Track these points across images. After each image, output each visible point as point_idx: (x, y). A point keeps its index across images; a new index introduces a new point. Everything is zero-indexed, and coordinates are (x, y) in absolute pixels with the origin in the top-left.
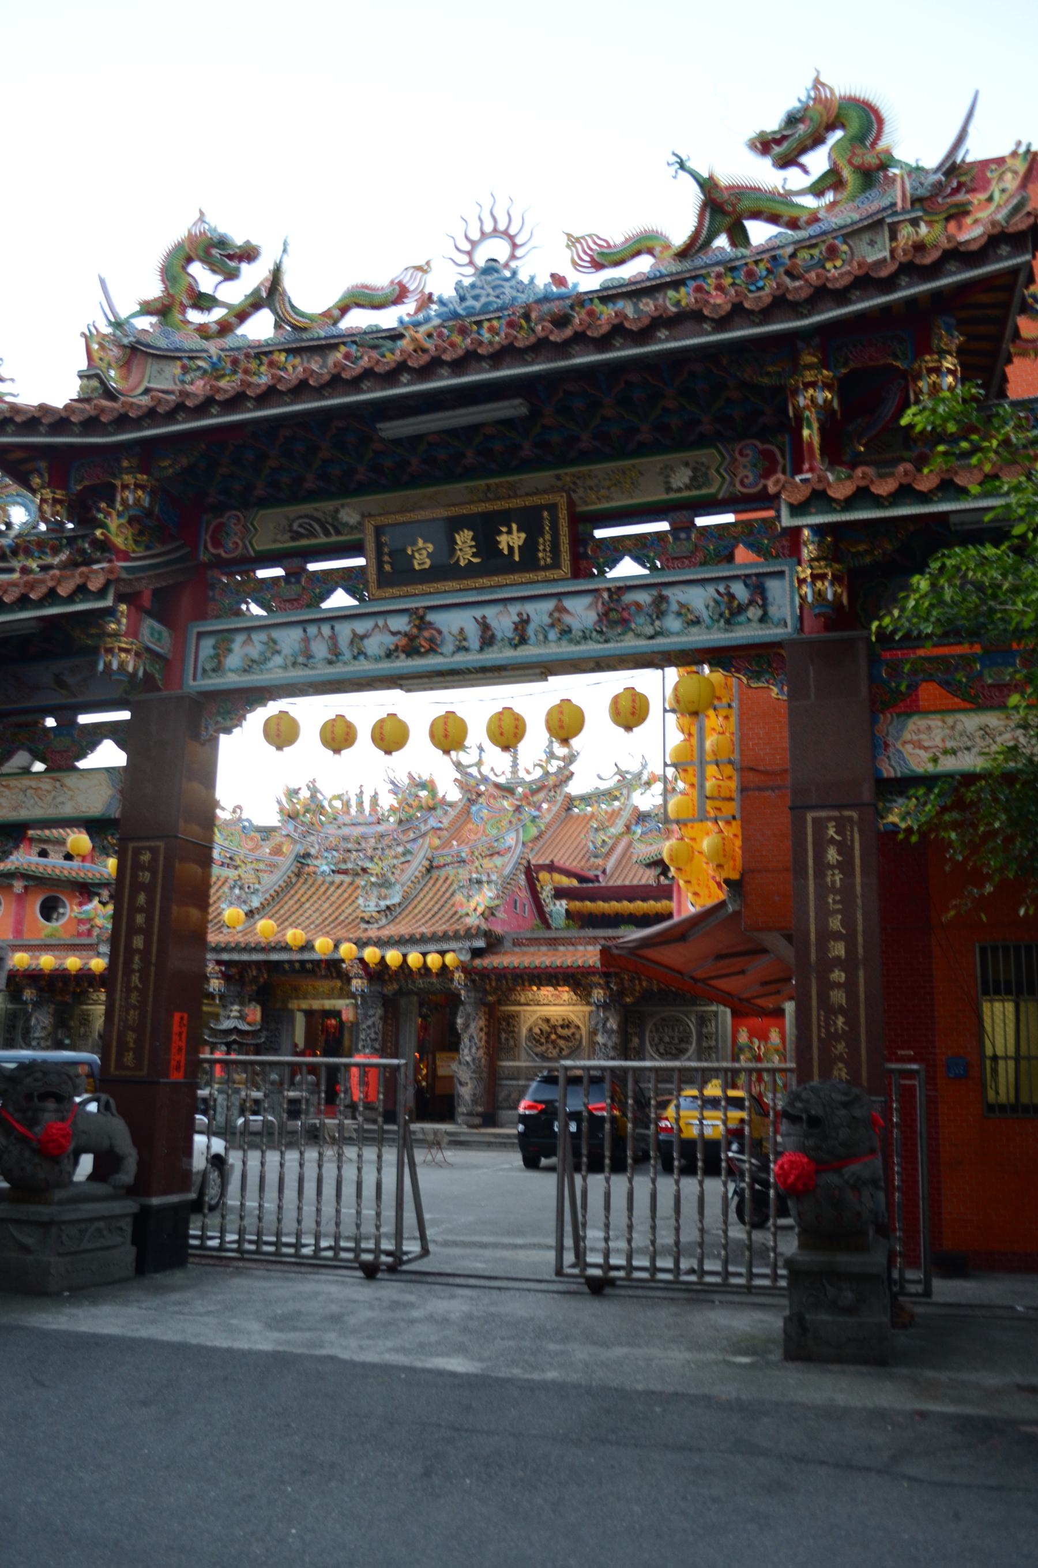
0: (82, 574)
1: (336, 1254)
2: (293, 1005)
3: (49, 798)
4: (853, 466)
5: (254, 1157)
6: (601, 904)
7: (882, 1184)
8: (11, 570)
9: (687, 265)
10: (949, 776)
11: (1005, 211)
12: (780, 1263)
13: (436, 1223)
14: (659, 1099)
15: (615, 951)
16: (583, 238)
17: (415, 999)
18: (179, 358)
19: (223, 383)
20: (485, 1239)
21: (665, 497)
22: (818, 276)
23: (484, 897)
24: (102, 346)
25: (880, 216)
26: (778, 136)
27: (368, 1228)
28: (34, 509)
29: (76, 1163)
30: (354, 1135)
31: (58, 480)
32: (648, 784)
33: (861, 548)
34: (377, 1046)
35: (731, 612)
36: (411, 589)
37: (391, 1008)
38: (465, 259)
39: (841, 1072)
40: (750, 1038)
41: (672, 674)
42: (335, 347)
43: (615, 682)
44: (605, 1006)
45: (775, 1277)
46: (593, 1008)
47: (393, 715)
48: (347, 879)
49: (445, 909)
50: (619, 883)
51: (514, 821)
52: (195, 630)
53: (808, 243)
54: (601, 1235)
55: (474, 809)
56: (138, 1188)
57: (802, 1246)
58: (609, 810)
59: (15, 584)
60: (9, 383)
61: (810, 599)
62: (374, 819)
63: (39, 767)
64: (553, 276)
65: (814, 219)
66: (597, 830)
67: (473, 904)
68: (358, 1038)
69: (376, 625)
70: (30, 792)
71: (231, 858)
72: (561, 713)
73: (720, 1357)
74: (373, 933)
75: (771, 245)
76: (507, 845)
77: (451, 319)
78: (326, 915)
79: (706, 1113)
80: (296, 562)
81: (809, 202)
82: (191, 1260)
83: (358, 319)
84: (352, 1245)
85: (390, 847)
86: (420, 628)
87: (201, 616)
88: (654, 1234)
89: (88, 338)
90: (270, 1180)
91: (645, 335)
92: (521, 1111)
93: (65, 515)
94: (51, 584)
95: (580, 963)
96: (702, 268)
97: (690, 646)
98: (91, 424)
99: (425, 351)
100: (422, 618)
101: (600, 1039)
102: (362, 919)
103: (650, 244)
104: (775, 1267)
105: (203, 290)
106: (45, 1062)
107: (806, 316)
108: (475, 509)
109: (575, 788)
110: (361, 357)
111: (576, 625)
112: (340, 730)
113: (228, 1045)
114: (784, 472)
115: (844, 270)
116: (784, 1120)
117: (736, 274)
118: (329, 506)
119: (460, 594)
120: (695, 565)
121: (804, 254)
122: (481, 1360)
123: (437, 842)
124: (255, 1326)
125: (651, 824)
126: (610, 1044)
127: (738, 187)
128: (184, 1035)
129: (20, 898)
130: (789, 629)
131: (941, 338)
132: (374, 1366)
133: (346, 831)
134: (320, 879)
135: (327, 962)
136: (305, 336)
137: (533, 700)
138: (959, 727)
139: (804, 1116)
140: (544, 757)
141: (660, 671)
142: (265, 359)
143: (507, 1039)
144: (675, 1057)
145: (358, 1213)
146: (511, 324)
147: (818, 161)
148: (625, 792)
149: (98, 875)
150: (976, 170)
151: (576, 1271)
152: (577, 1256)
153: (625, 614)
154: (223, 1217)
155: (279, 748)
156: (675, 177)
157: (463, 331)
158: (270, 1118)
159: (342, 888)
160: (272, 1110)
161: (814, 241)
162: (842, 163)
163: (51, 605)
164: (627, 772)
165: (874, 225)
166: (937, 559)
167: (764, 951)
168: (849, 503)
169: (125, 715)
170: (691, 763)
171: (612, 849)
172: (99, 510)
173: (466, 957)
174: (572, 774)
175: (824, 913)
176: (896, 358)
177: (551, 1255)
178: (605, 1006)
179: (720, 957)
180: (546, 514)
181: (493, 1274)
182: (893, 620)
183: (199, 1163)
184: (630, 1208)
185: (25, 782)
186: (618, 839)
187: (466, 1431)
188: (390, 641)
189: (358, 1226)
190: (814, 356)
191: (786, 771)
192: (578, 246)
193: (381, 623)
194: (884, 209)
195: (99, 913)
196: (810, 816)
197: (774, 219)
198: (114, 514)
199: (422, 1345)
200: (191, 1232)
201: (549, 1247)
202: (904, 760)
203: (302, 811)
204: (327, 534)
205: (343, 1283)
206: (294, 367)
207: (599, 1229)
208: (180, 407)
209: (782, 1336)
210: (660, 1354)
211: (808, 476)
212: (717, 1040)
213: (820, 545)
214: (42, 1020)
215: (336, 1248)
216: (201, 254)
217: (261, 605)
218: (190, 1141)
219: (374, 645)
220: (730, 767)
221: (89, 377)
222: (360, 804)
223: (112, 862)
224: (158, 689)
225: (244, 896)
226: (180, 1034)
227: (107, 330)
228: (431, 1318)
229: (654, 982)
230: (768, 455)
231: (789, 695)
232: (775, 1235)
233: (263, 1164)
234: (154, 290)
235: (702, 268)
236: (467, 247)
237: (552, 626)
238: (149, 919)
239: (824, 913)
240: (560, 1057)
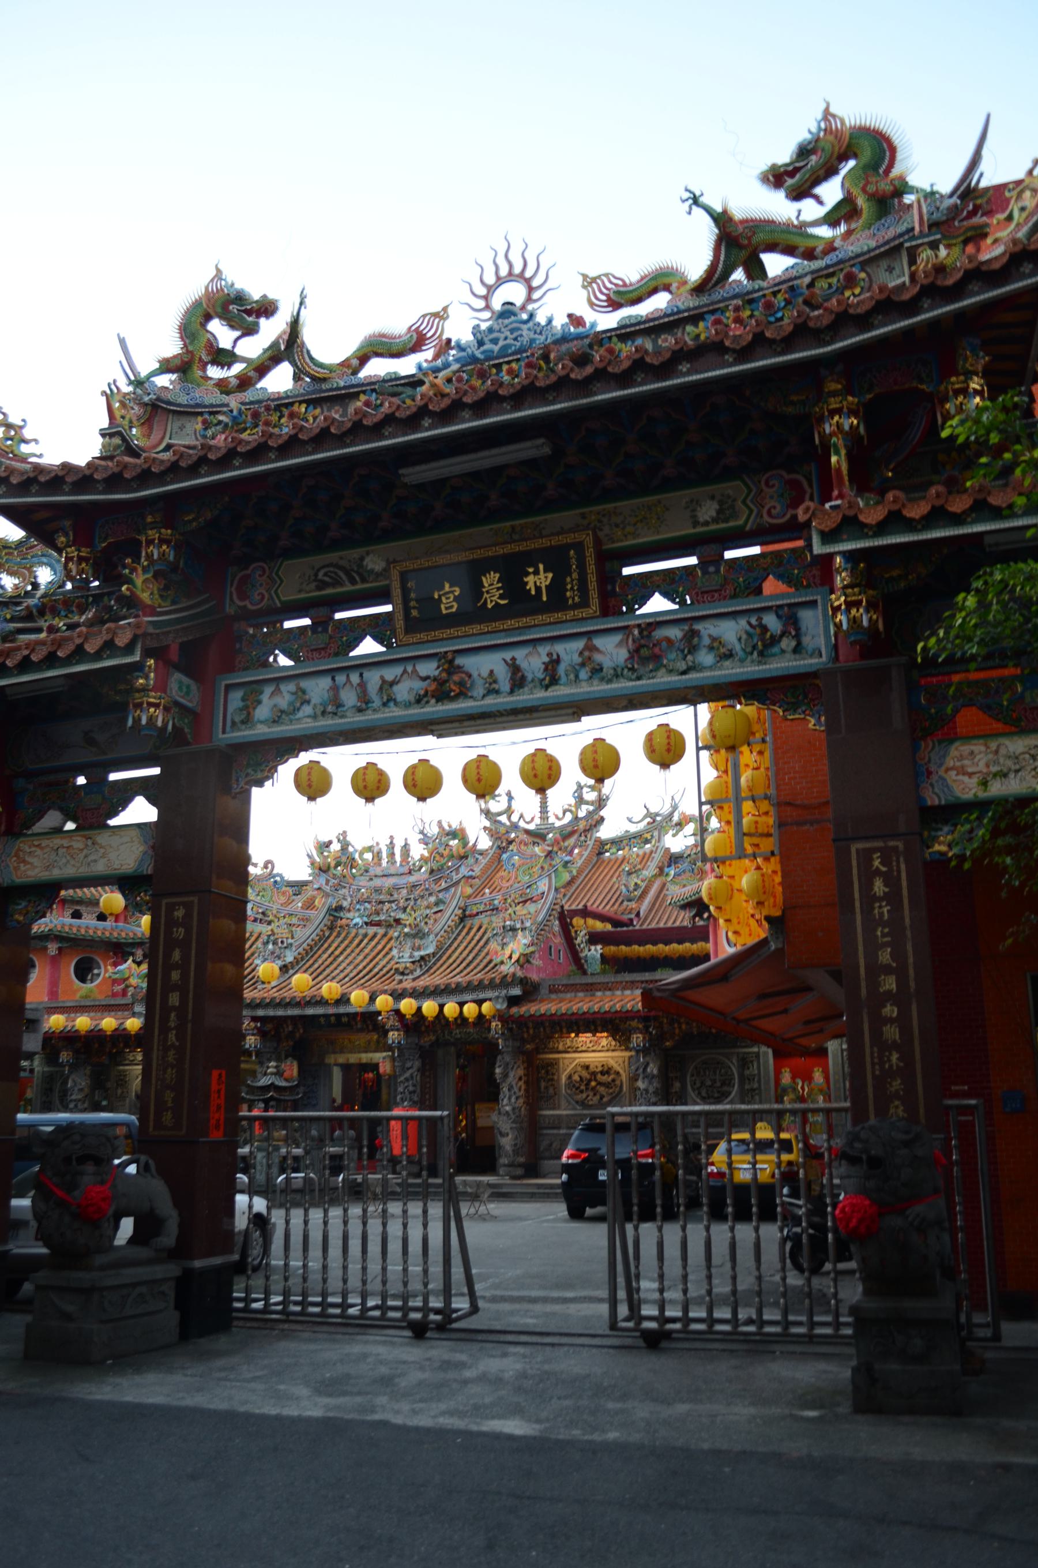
0: (108, 630)
1: (384, 1314)
2: (330, 1059)
3: (82, 856)
4: (882, 493)
5: (297, 1216)
6: (636, 947)
7: (947, 1224)
8: (39, 630)
9: (705, 299)
10: (1000, 802)
11: (1025, 229)
12: (844, 1309)
13: (484, 1278)
14: (709, 1142)
15: (657, 994)
16: (599, 277)
17: (453, 1049)
18: (201, 414)
19: (244, 436)
20: (534, 1293)
21: (692, 531)
22: (838, 301)
23: (519, 944)
24: (123, 405)
25: (897, 242)
26: (791, 168)
27: (416, 1285)
28: (59, 568)
29: (117, 1227)
30: (399, 1190)
31: (82, 537)
32: (680, 825)
33: (895, 573)
34: (416, 1099)
35: (764, 644)
36: (438, 634)
37: (428, 1059)
38: (481, 304)
39: (898, 1110)
40: (793, 1078)
41: (704, 710)
42: (355, 396)
43: (647, 720)
44: (645, 1051)
45: (837, 1325)
46: (633, 1053)
47: (424, 762)
48: (381, 931)
49: (480, 958)
50: (653, 926)
51: (546, 867)
52: (224, 683)
53: (825, 272)
54: (655, 1285)
55: (505, 856)
56: (180, 1251)
57: (867, 1292)
58: (641, 852)
59: (42, 643)
60: (33, 443)
61: (845, 626)
62: (406, 870)
63: (70, 826)
64: (570, 316)
65: (830, 247)
66: (629, 873)
67: (507, 952)
68: (396, 1090)
69: (405, 671)
70: (61, 851)
71: (263, 913)
72: (596, 752)
73: (787, 1411)
74: (408, 984)
75: (788, 276)
76: (540, 891)
77: (469, 364)
78: (360, 967)
79: (759, 1157)
80: (323, 611)
81: (824, 232)
82: (235, 1323)
83: (377, 368)
84: (399, 1303)
85: (422, 897)
86: (450, 674)
87: (229, 667)
88: (710, 1283)
89: (109, 397)
90: (319, 1240)
91: (667, 368)
92: (564, 1160)
93: (90, 572)
94: (78, 641)
95: (618, 1007)
96: (719, 302)
97: (723, 680)
98: (115, 481)
99: (444, 395)
100: (451, 662)
101: (641, 1084)
102: (397, 970)
103: (666, 280)
104: (837, 1315)
105: (221, 346)
106: (82, 1123)
107: (829, 344)
108: (500, 551)
109: (605, 832)
110: (381, 405)
111: (607, 663)
112: (372, 777)
113: (266, 1102)
114: (812, 499)
115: (862, 297)
116: (843, 1162)
117: (754, 306)
118: (354, 554)
119: (488, 636)
120: (725, 598)
121: (822, 284)
122: (538, 1421)
123: (469, 891)
124: (304, 1391)
125: (684, 865)
126: (651, 1090)
127: (752, 220)
128: (223, 1093)
129: (55, 961)
130: (824, 659)
131: (966, 359)
132: (428, 1431)
133: (377, 882)
134: (354, 932)
135: (363, 1014)
136: (324, 386)
137: (565, 741)
138: (1003, 751)
139: (864, 1157)
140: (573, 801)
141: (692, 708)
142: (286, 412)
143: (546, 1088)
144: (718, 1101)
145: (405, 1270)
146: (529, 365)
147: (831, 191)
148: (656, 834)
149: (131, 935)
150: (991, 192)
151: (631, 1324)
152: (631, 1308)
153: (657, 650)
154: (267, 1278)
155: (312, 798)
156: (690, 213)
157: (482, 375)
158: (311, 1175)
159: (376, 940)
160: (311, 1166)
161: (831, 270)
162: (856, 191)
163: (78, 663)
164: (657, 815)
165: (891, 252)
166: (979, 577)
167: (808, 989)
168: (881, 528)
169: (156, 771)
170: (727, 800)
171: (645, 893)
172: (125, 567)
173: (502, 1006)
174: (602, 819)
175: (873, 947)
176: (922, 382)
177: (604, 1309)
178: (645, 1051)
179: (763, 996)
180: (572, 552)
181: (544, 1330)
182: (939, 641)
183: (241, 1222)
184: (684, 1258)
185: (57, 841)
186: (650, 883)
187: (529, 1498)
188: (419, 686)
189: (405, 1284)
190: (838, 382)
191: (827, 803)
192: (594, 285)
193: (410, 669)
194: (901, 235)
195: (134, 972)
196: (854, 848)
197: (789, 250)
198: (140, 570)
199: (476, 1407)
200: (235, 1295)
201: (600, 1300)
202: (947, 786)
203: (333, 864)
204: (353, 582)
205: (393, 1344)
206: (315, 418)
207: (652, 1280)
208: (203, 460)
209: (850, 1387)
210: (727, 1410)
211: (839, 502)
212: (759, 1082)
213: (853, 573)
214: (79, 1082)
215: (383, 1308)
216: (219, 310)
217: (290, 656)
218: (232, 1202)
219: (403, 691)
220: (766, 802)
221: (111, 435)
223: (146, 920)
224: (188, 744)
225: (278, 952)
226: (219, 1091)
227: (126, 389)
228: (483, 1378)
229: (698, 1021)
230: (794, 485)
231: (827, 725)
232: (835, 1280)
233: (306, 1222)
234: (172, 347)
235: (719, 302)
236: (483, 291)
237: (583, 665)
238: (185, 976)
239: (873, 947)
240: (602, 1105)
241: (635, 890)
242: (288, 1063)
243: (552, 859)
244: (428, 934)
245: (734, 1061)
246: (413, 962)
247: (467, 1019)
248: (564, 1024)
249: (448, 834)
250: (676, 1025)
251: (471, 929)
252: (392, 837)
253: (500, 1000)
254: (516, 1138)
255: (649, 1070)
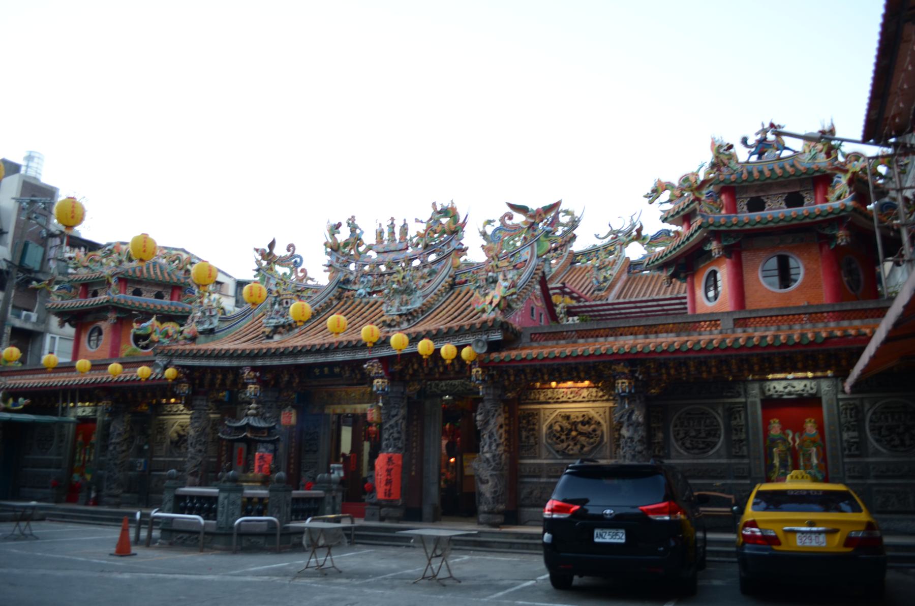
37: (415, 410)
40: (783, 429)
44: (631, 397)
66: (599, 269)
67: (488, 298)
76: (523, 260)
92: (547, 514)
126: (637, 438)
134: (358, 301)
143: (527, 437)
164: (619, 232)
174: (574, 237)
178: (631, 397)
212: (747, 433)
222: (392, 233)
241: (604, 282)
242: (287, 411)
243: (535, 230)
244: (415, 290)
245: (720, 411)
246: (400, 315)
247: (443, 360)
248: (545, 370)
249: (439, 213)
250: (663, 371)
251: (459, 294)
252: (392, 219)
253: (480, 344)
254: (496, 486)
255: (634, 417)
